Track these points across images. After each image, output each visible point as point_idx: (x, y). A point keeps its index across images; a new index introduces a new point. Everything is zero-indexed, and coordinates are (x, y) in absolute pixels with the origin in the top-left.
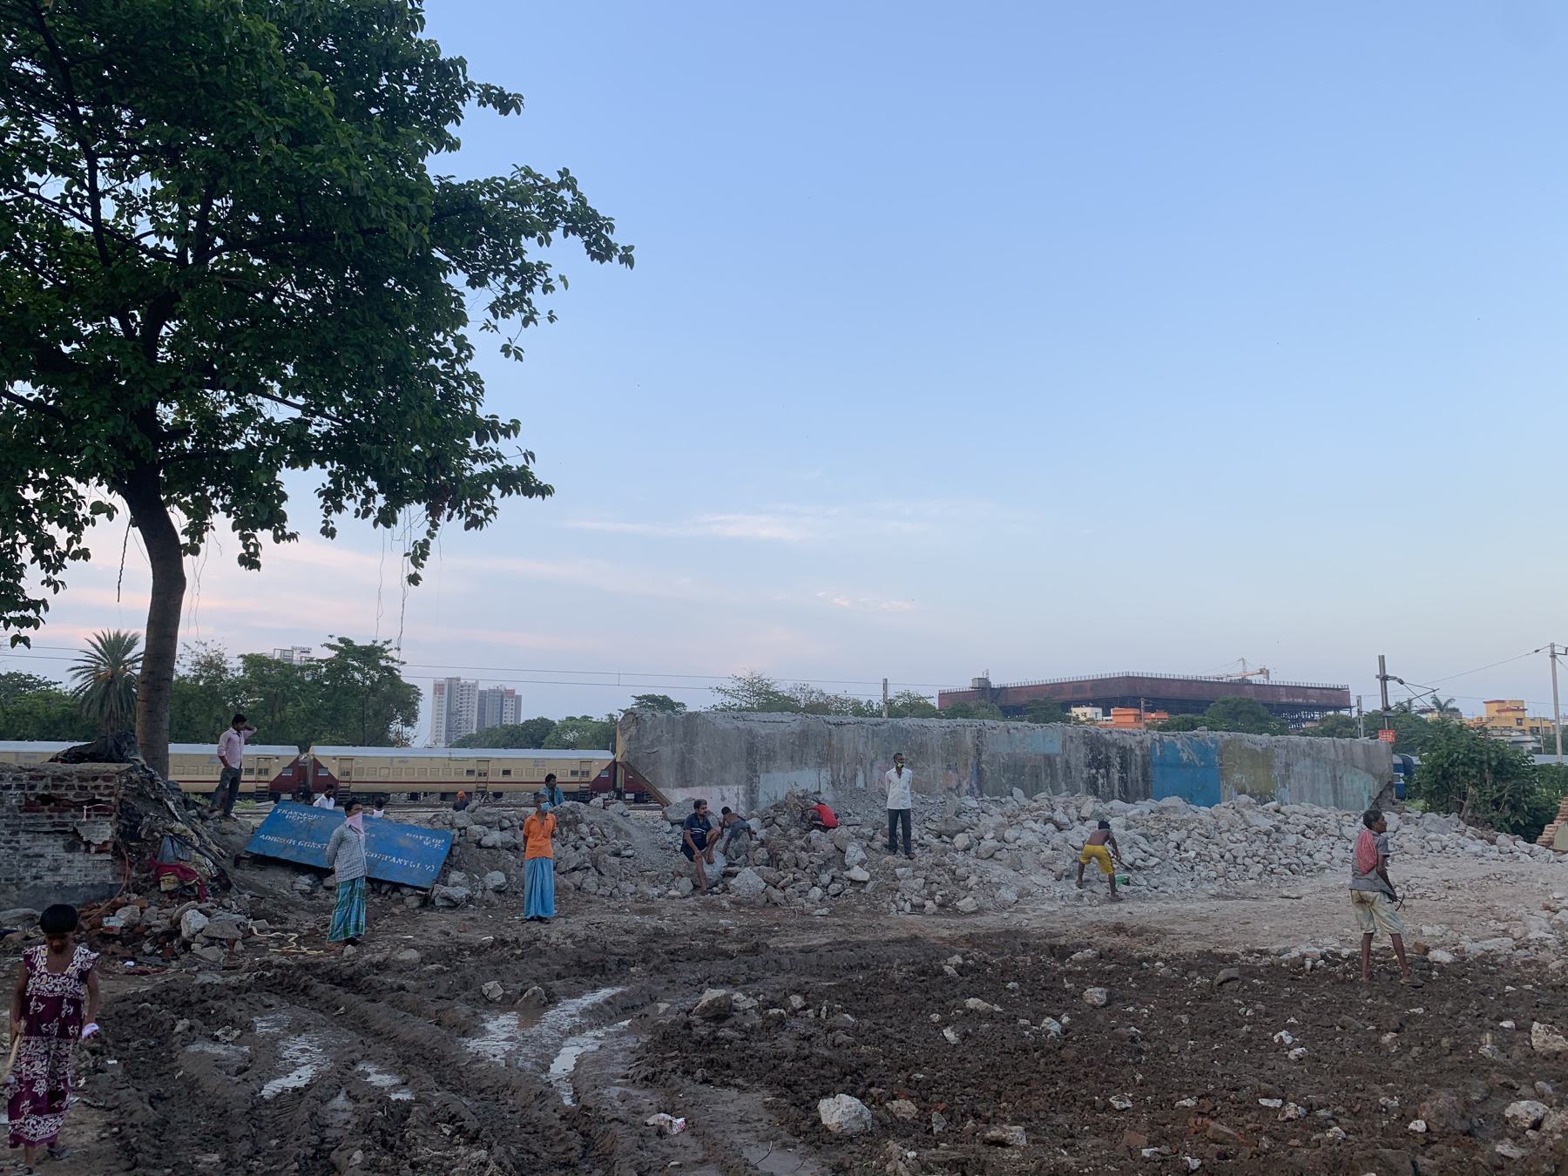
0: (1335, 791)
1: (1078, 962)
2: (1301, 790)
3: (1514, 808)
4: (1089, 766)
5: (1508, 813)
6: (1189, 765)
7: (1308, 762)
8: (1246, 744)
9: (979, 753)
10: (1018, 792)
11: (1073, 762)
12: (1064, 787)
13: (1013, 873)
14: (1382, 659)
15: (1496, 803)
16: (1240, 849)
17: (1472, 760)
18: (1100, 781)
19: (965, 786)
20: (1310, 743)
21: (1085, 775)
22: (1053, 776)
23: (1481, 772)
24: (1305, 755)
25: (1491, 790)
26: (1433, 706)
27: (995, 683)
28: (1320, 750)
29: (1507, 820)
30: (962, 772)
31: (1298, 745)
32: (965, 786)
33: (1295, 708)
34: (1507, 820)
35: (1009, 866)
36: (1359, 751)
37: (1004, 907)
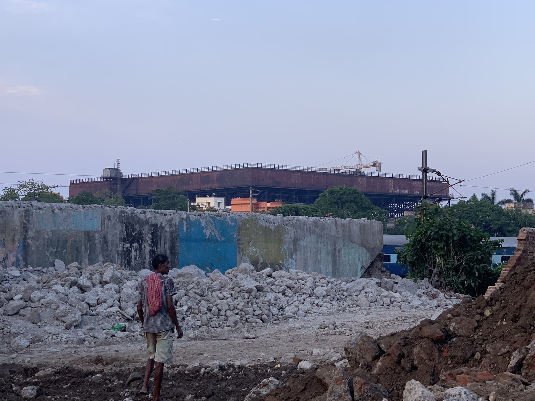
0: (334, 263)
1: (38, 377)
2: (306, 260)
3: (470, 273)
4: (124, 240)
5: (464, 278)
6: (211, 240)
7: (313, 238)
8: (262, 223)
9: (25, 229)
10: (59, 263)
11: (110, 238)
12: (101, 258)
13: (31, 325)
14: (425, 153)
15: (456, 270)
16: (223, 304)
17: (442, 235)
18: (133, 254)
19: (12, 258)
20: (316, 222)
21: (120, 249)
22: (92, 250)
23: (448, 245)
24: (311, 232)
25: (453, 261)
26: (512, 198)
27: (127, 172)
28: (323, 228)
29: (463, 283)
30: (9, 246)
31: (305, 224)
32: (12, 258)
33: (401, 199)
34: (463, 283)
35: (29, 320)
36: (355, 229)
37: (17, 350)
